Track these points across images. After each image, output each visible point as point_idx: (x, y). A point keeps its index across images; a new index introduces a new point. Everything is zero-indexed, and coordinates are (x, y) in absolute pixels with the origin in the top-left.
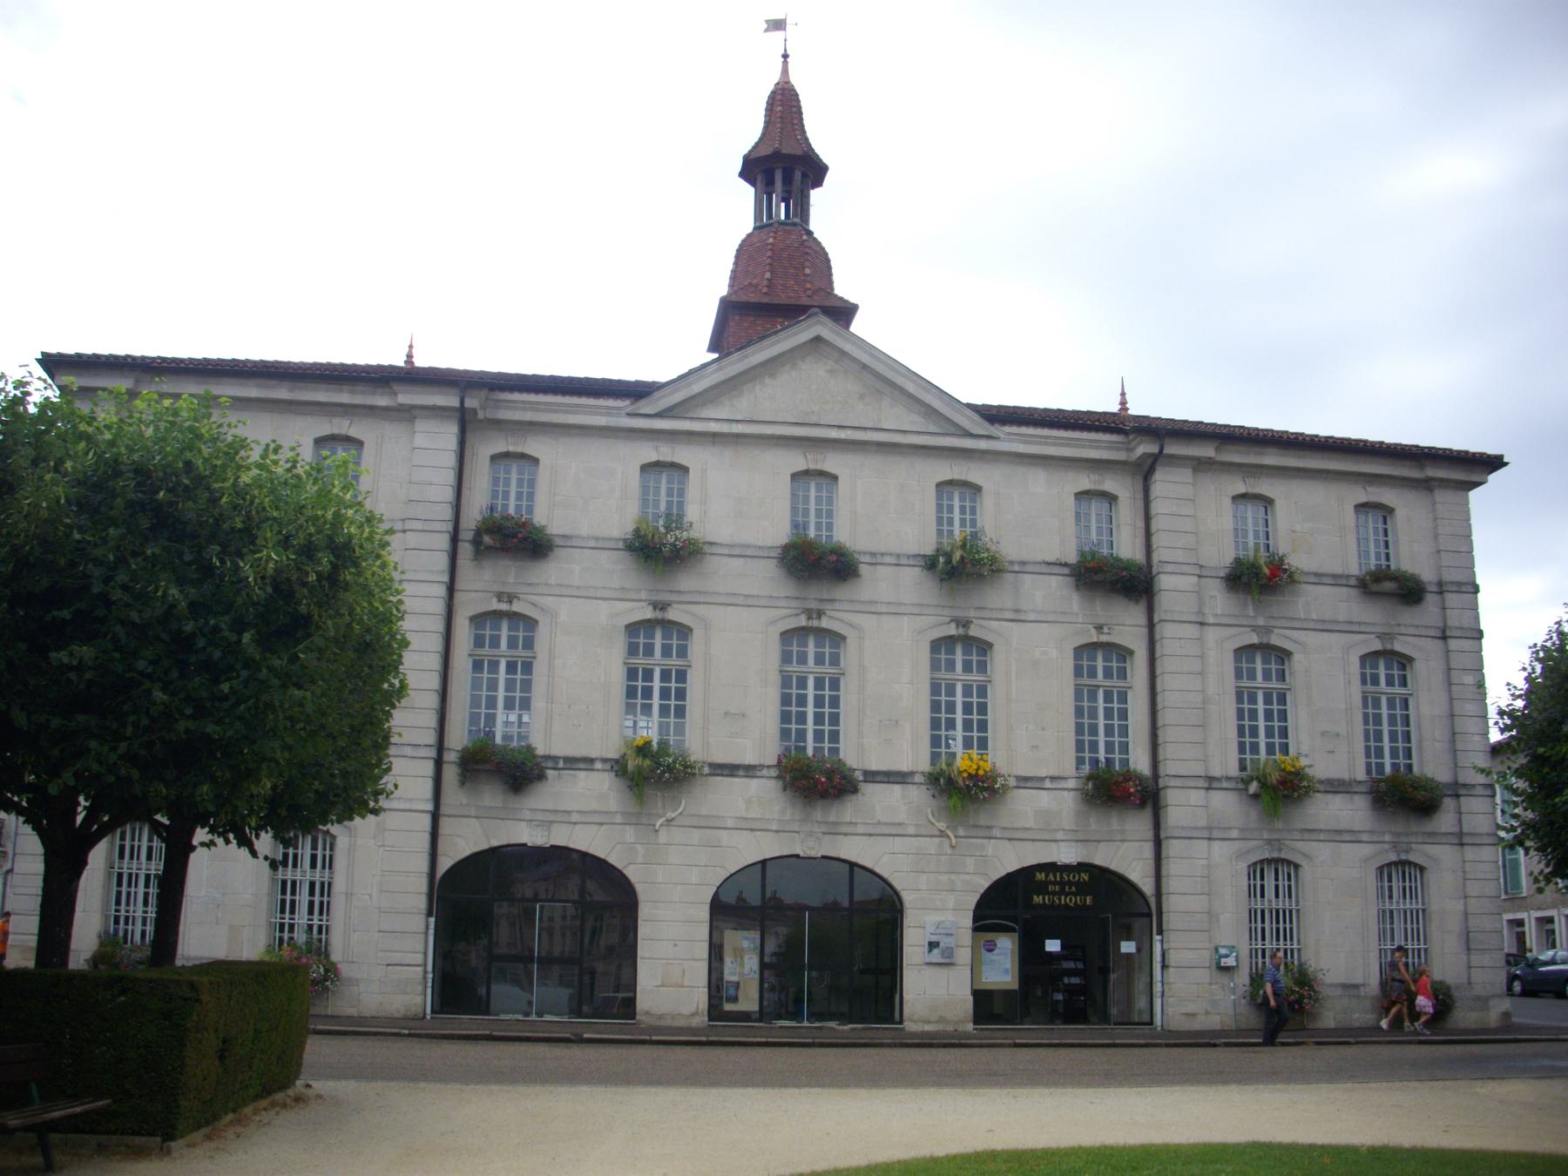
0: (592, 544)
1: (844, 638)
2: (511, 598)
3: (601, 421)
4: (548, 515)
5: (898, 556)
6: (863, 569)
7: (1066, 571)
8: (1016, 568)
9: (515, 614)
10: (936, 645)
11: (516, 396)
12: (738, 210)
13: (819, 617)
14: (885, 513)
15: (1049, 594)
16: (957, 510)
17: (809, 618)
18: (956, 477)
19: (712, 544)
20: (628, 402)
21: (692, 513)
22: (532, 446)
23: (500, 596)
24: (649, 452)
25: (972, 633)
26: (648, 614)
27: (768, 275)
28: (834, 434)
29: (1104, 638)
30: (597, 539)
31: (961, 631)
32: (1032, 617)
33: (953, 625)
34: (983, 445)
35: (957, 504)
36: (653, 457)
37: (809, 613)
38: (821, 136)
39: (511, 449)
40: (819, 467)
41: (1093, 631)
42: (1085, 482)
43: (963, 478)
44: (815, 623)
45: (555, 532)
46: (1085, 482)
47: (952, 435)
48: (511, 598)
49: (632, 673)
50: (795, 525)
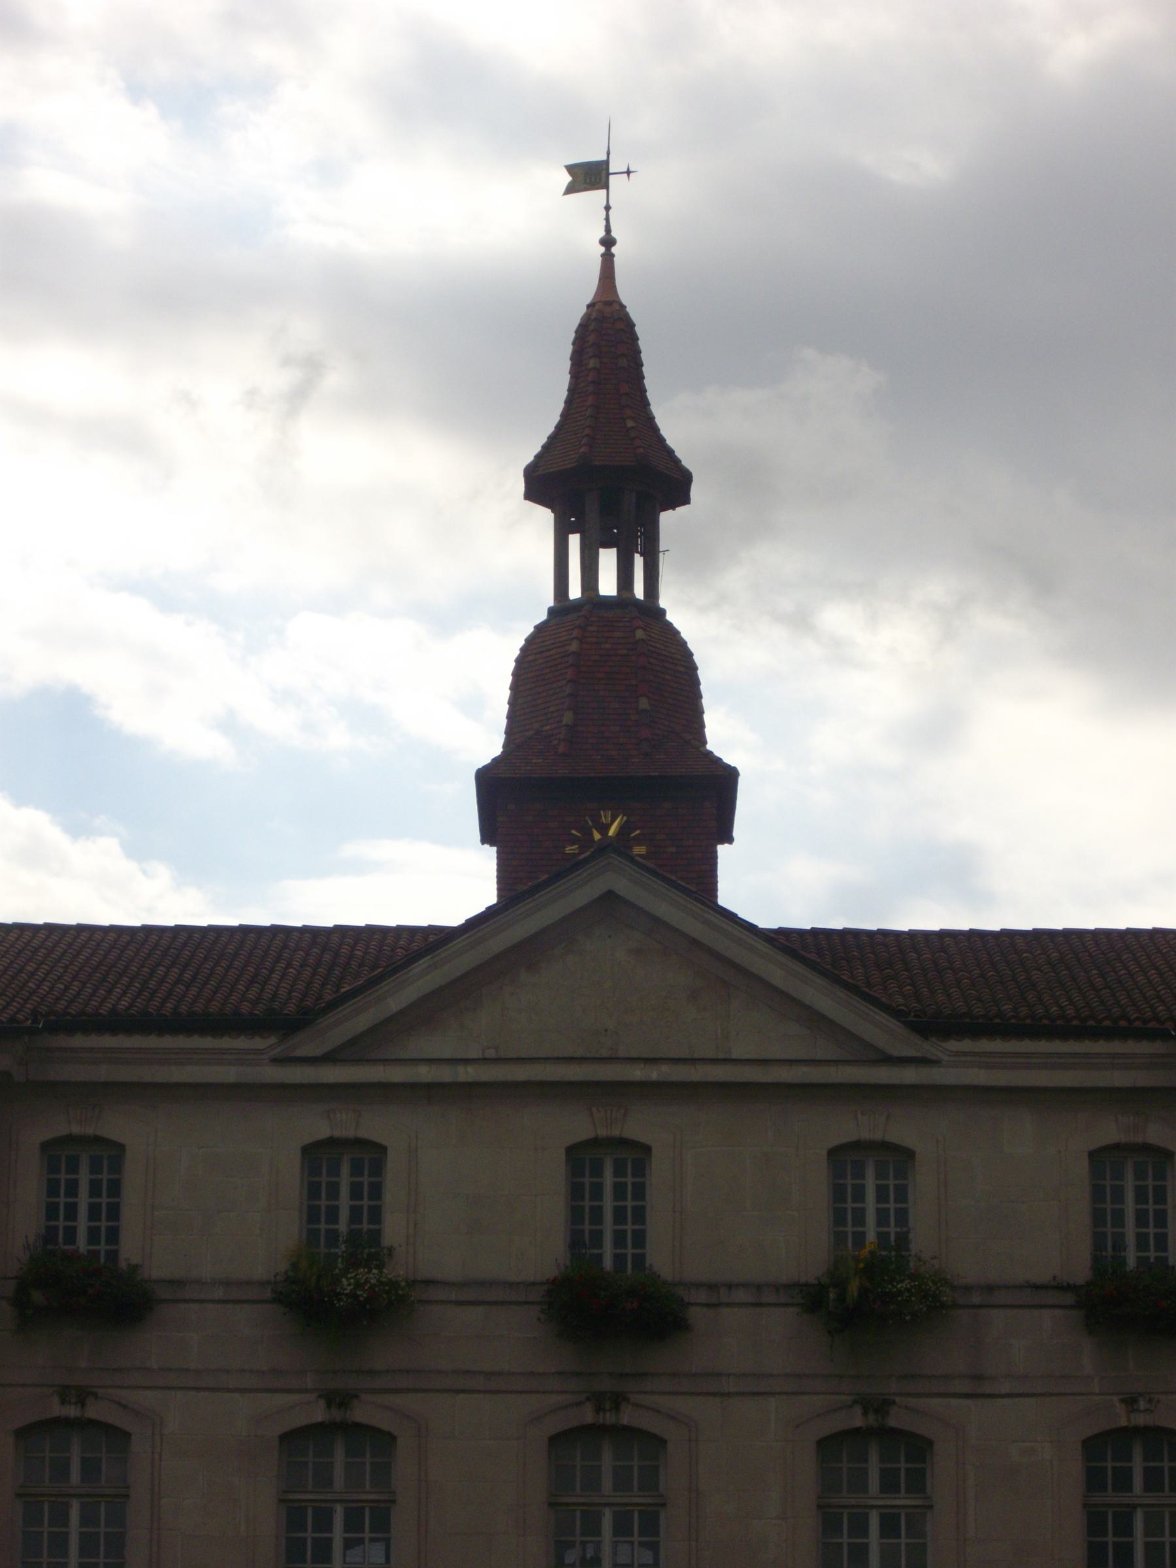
0: (219, 1293)
1: (663, 1442)
2: (82, 1395)
3: (229, 1074)
4: (148, 1243)
5: (759, 1287)
6: (696, 1315)
7: (1069, 1299)
8: (976, 1299)
9: (92, 1422)
10: (828, 1446)
11: (79, 1041)
12: (520, 562)
13: (616, 1408)
14: (739, 1208)
15: (1029, 1341)
16: (1130, 1196)
17: (599, 1409)
18: (865, 1135)
19: (428, 1283)
20: (272, 1040)
21: (393, 1229)
22: (116, 1125)
23: (65, 1393)
24: (317, 1125)
25: (892, 1422)
26: (319, 1414)
27: (568, 717)
28: (637, 1073)
29: (1140, 1420)
30: (228, 1283)
31: (872, 1420)
32: (1005, 1388)
33: (858, 1410)
34: (910, 1075)
35: (1129, 1184)
36: (322, 1130)
37: (598, 1400)
38: (681, 419)
39: (76, 1129)
40: (616, 1132)
41: (1120, 1408)
42: (1110, 1130)
43: (878, 1136)
44: (609, 1418)
45: (156, 1274)
46: (1110, 1130)
47: (836, 1062)
48: (82, 1395)
49: (294, 1516)
50: (575, 1242)
